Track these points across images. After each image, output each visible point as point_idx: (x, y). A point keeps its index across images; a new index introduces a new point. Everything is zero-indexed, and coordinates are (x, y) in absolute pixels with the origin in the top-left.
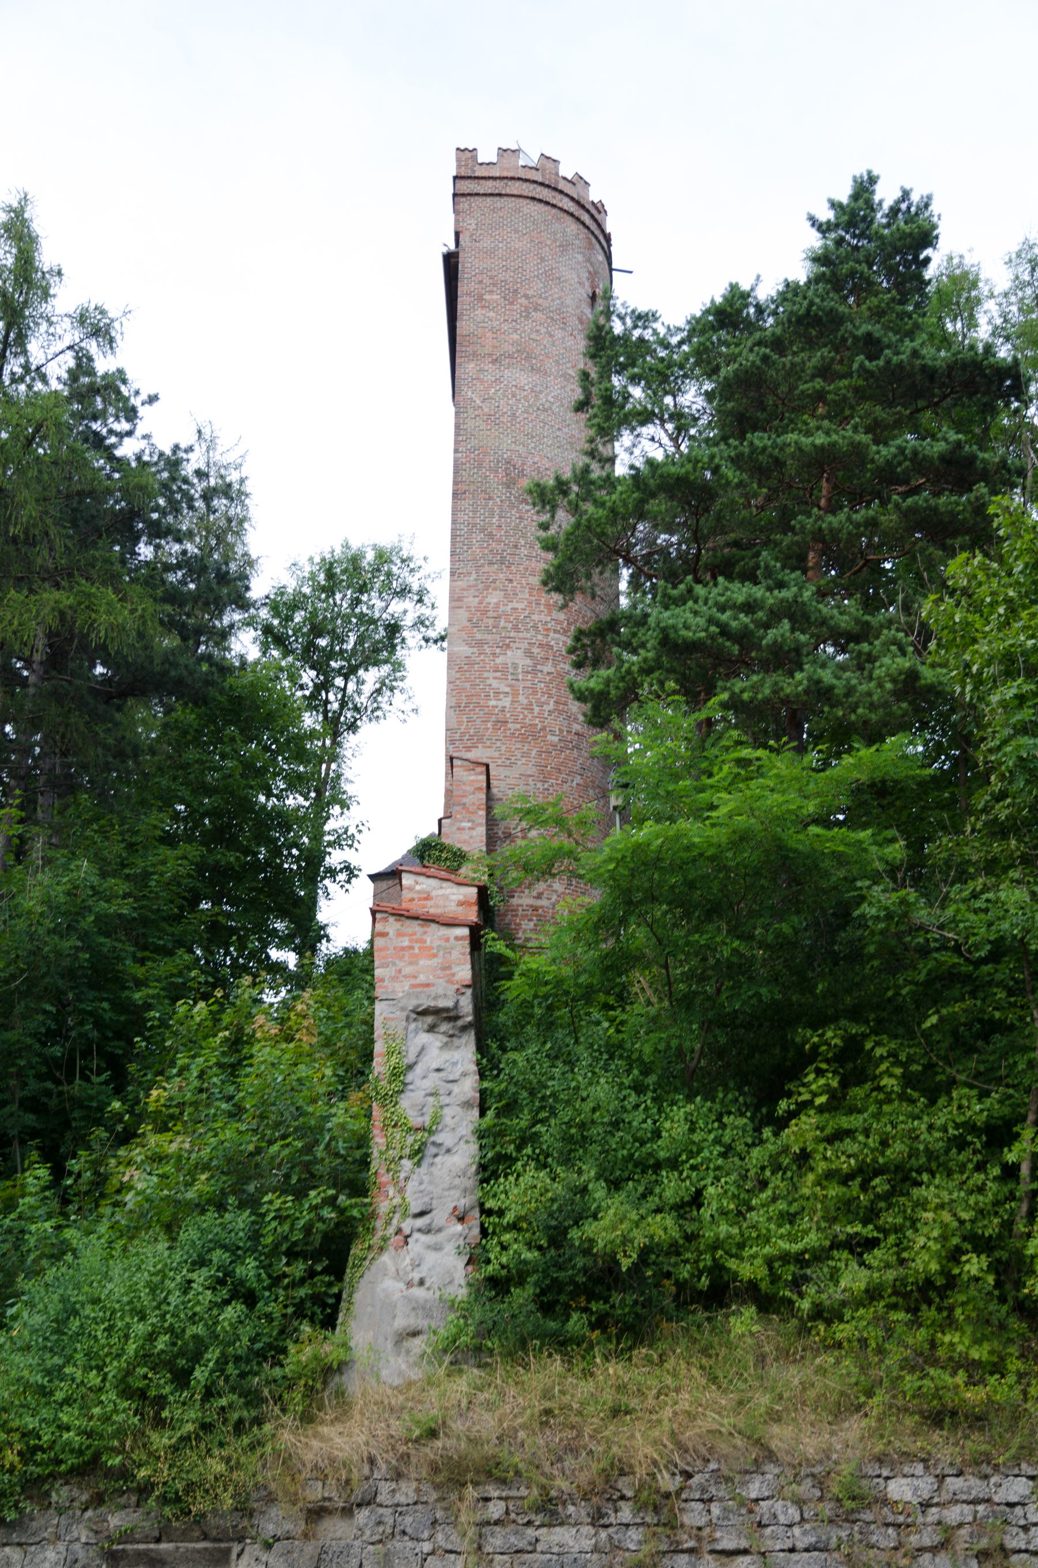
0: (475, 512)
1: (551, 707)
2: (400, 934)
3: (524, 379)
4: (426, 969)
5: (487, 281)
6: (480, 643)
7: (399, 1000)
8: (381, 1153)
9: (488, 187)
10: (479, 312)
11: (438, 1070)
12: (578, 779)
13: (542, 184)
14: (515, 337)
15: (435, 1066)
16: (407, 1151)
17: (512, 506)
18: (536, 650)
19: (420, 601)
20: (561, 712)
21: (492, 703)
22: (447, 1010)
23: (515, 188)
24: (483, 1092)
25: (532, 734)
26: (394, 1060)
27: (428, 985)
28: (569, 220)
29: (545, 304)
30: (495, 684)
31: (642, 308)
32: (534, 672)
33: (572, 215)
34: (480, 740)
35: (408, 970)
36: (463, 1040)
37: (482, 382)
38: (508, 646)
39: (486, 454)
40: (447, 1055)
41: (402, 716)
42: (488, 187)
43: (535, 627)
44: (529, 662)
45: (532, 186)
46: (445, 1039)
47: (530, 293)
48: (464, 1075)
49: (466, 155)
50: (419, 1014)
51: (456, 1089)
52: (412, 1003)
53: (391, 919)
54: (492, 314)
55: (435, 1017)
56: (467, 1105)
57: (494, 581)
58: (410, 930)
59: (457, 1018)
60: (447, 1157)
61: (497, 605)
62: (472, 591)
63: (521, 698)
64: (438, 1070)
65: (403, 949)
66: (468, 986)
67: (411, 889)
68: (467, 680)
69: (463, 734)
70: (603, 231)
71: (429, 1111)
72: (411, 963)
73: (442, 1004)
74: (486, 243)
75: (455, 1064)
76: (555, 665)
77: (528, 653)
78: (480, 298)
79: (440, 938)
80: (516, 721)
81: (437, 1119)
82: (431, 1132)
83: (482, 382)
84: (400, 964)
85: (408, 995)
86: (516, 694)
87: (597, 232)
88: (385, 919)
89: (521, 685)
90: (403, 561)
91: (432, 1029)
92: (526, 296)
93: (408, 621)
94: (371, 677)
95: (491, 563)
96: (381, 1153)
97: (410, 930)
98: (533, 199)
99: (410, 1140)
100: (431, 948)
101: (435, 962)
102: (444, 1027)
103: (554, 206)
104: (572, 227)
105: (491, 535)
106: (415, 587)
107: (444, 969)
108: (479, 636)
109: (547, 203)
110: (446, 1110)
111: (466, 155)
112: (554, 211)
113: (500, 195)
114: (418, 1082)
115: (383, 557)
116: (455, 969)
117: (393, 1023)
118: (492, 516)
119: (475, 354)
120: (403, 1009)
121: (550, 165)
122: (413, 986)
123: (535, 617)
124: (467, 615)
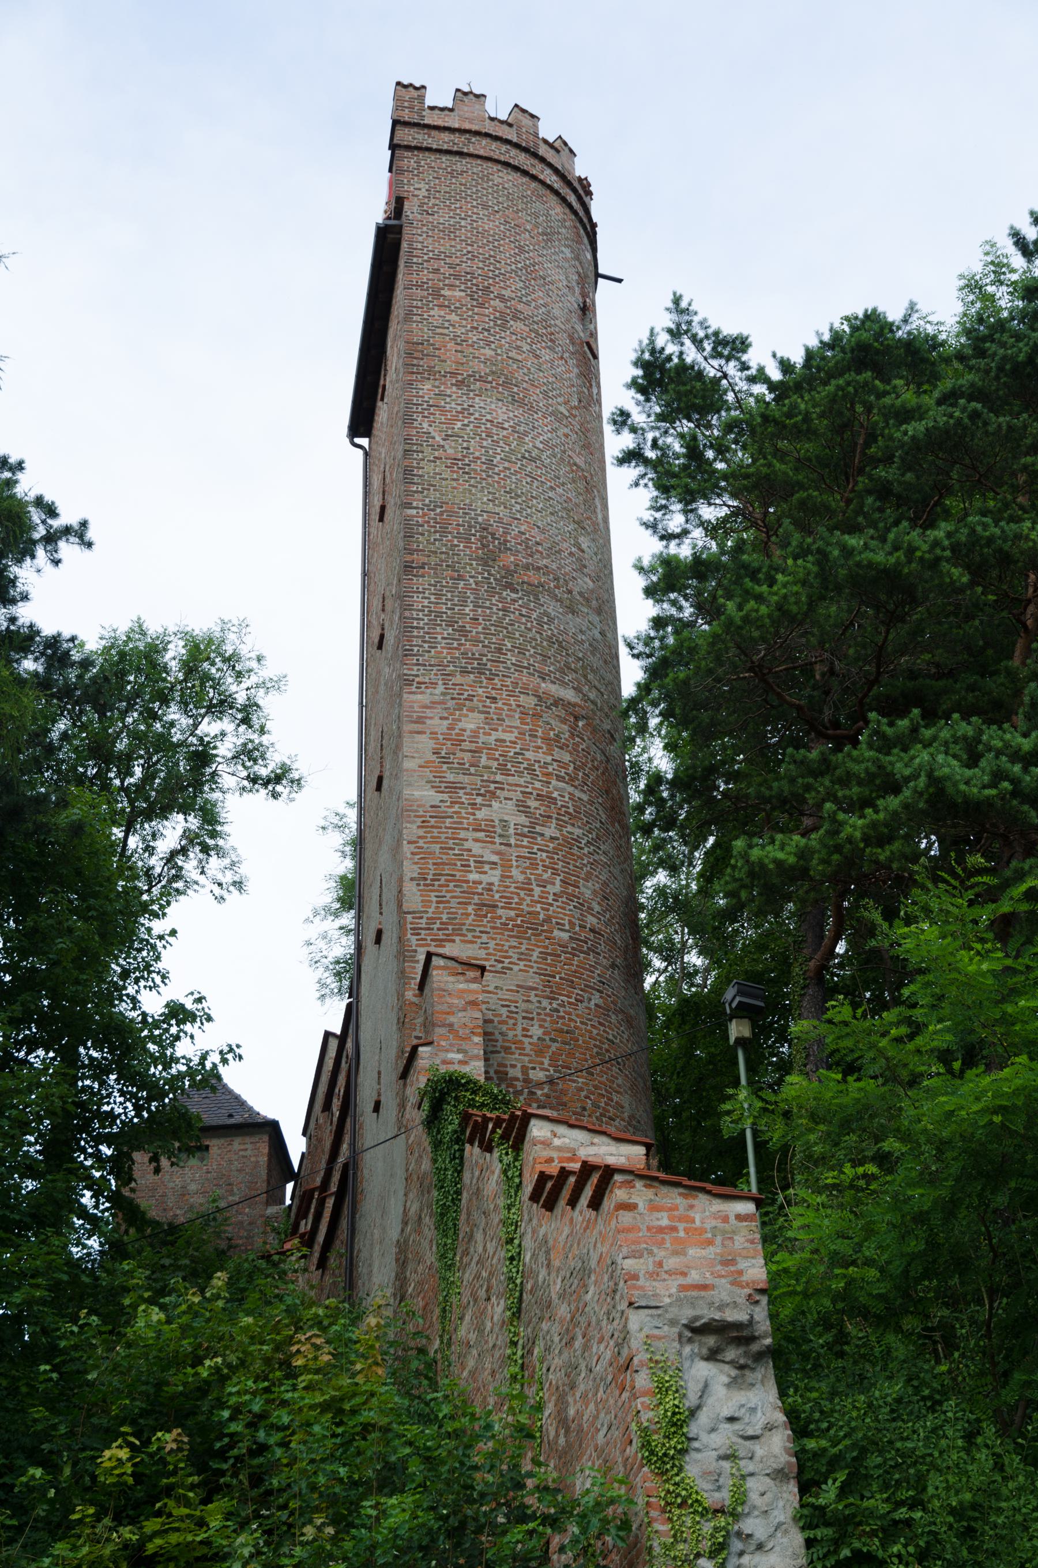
0: (438, 596)
1: (557, 888)
2: (654, 1208)
3: (502, 413)
4: (699, 1261)
5: (445, 270)
6: (453, 788)
7: (665, 1308)
8: (667, 1548)
9: (444, 140)
10: (436, 312)
11: (732, 1419)
12: (596, 999)
13: (517, 146)
14: (488, 352)
15: (726, 1412)
16: (706, 1545)
17: (491, 591)
18: (533, 804)
19: (246, 721)
20: (571, 897)
21: (473, 877)
22: (738, 1326)
23: (482, 146)
24: (800, 1455)
25: (530, 927)
26: (670, 1401)
27: (704, 1287)
28: (553, 199)
29: (527, 311)
30: (477, 849)
31: (729, 330)
32: (532, 835)
33: (556, 193)
34: (458, 932)
35: (671, 1263)
36: (758, 1375)
37: (443, 411)
38: (493, 794)
39: (452, 513)
40: (741, 1397)
41: (217, 890)
42: (444, 140)
43: (530, 769)
44: (523, 819)
45: (504, 148)
46: (734, 1372)
47: (507, 293)
48: (769, 1428)
49: (408, 93)
50: (695, 1331)
51: (759, 1450)
52: (686, 1314)
53: (639, 1184)
54: (453, 317)
55: (718, 1336)
56: (779, 1475)
57: (470, 698)
58: (667, 1202)
59: (752, 1339)
60: (757, 1558)
61: (475, 733)
62: (439, 710)
63: (515, 872)
64: (732, 1419)
65: (661, 1230)
66: (762, 1291)
67: (546, 1144)
68: (435, 840)
69: (431, 920)
70: (590, 219)
71: (727, 1482)
72: (675, 1253)
73: (732, 1316)
74: (443, 217)
75: (753, 1410)
76: (560, 827)
77: (522, 807)
78: (437, 293)
79: (715, 1216)
80: (508, 907)
81: (740, 1497)
82: (736, 1516)
83: (443, 411)
84: (660, 1254)
85: (679, 1302)
86: (506, 866)
87: (585, 220)
88: (629, 1184)
89: (514, 853)
90: (226, 660)
91: (713, 1356)
92: (501, 298)
93: (224, 749)
94: (172, 831)
95: (465, 672)
96: (667, 1548)
97: (667, 1202)
98: (506, 164)
99: (707, 1528)
100: (702, 1231)
101: (711, 1252)
102: (732, 1353)
103: (534, 178)
104: (558, 210)
105: (463, 631)
106: (241, 698)
107: (727, 1263)
108: (450, 777)
109: (525, 173)
110: (750, 1483)
111: (408, 93)
112: (534, 185)
113: (460, 154)
114: (704, 1438)
115: (199, 652)
116: (742, 1265)
117: (661, 1345)
118: (464, 603)
119: (431, 370)
120: (673, 1323)
121: (526, 121)
122: (683, 1288)
123: (529, 755)
124: (431, 744)
